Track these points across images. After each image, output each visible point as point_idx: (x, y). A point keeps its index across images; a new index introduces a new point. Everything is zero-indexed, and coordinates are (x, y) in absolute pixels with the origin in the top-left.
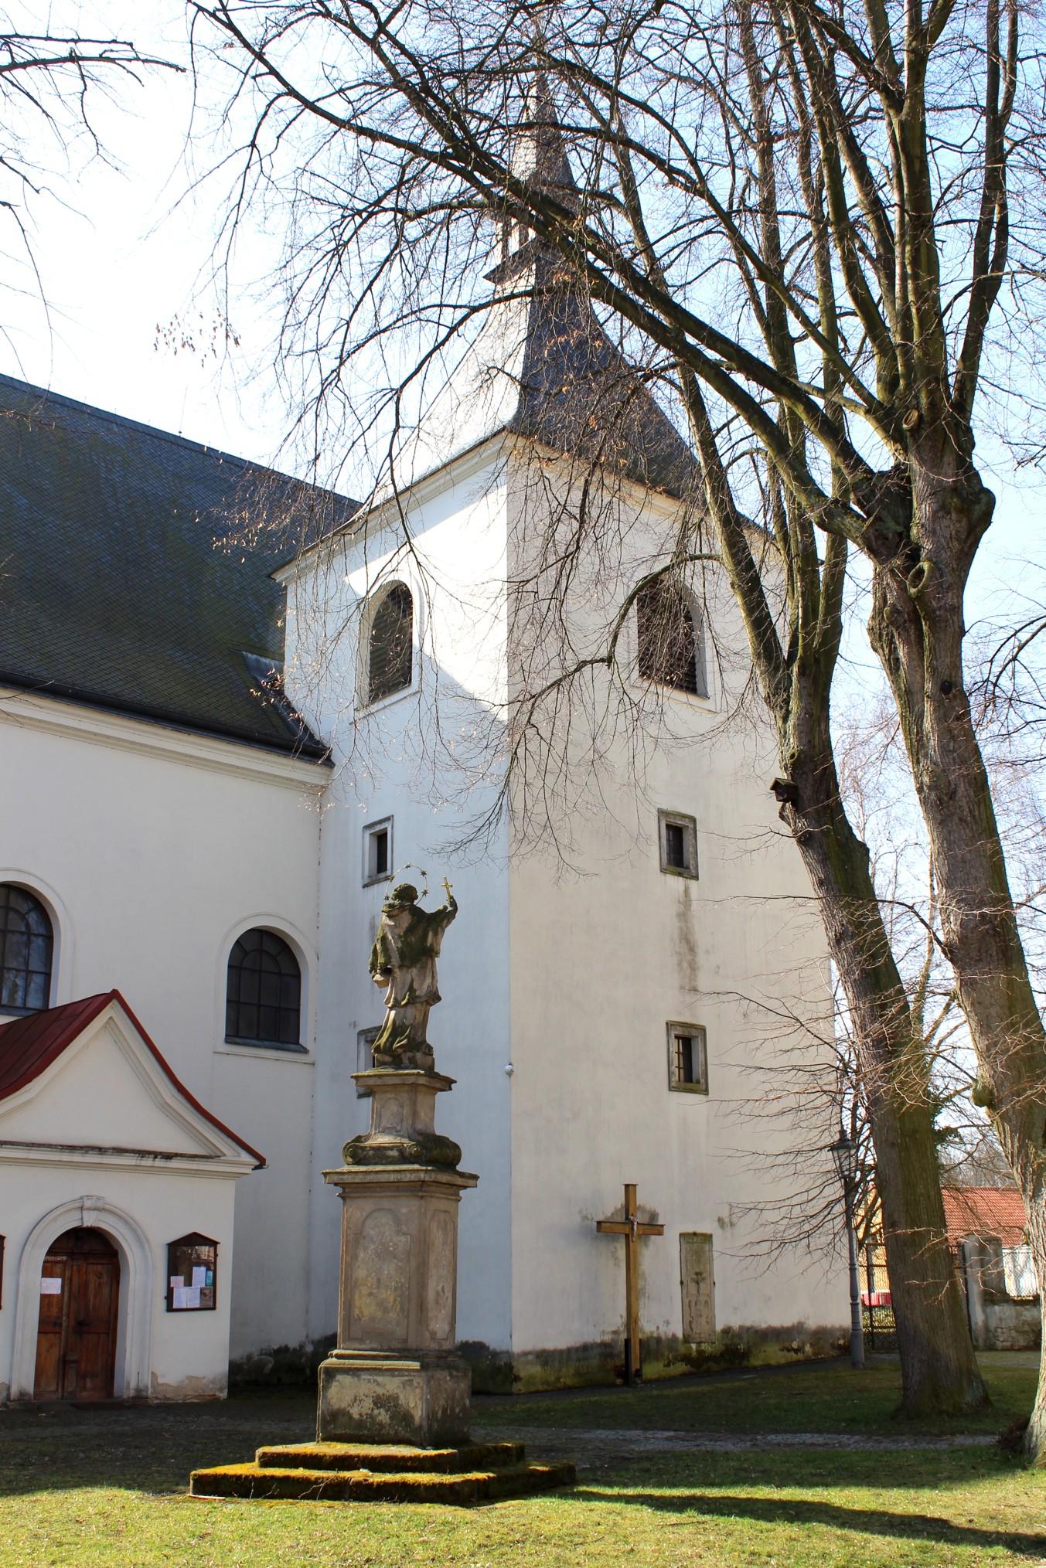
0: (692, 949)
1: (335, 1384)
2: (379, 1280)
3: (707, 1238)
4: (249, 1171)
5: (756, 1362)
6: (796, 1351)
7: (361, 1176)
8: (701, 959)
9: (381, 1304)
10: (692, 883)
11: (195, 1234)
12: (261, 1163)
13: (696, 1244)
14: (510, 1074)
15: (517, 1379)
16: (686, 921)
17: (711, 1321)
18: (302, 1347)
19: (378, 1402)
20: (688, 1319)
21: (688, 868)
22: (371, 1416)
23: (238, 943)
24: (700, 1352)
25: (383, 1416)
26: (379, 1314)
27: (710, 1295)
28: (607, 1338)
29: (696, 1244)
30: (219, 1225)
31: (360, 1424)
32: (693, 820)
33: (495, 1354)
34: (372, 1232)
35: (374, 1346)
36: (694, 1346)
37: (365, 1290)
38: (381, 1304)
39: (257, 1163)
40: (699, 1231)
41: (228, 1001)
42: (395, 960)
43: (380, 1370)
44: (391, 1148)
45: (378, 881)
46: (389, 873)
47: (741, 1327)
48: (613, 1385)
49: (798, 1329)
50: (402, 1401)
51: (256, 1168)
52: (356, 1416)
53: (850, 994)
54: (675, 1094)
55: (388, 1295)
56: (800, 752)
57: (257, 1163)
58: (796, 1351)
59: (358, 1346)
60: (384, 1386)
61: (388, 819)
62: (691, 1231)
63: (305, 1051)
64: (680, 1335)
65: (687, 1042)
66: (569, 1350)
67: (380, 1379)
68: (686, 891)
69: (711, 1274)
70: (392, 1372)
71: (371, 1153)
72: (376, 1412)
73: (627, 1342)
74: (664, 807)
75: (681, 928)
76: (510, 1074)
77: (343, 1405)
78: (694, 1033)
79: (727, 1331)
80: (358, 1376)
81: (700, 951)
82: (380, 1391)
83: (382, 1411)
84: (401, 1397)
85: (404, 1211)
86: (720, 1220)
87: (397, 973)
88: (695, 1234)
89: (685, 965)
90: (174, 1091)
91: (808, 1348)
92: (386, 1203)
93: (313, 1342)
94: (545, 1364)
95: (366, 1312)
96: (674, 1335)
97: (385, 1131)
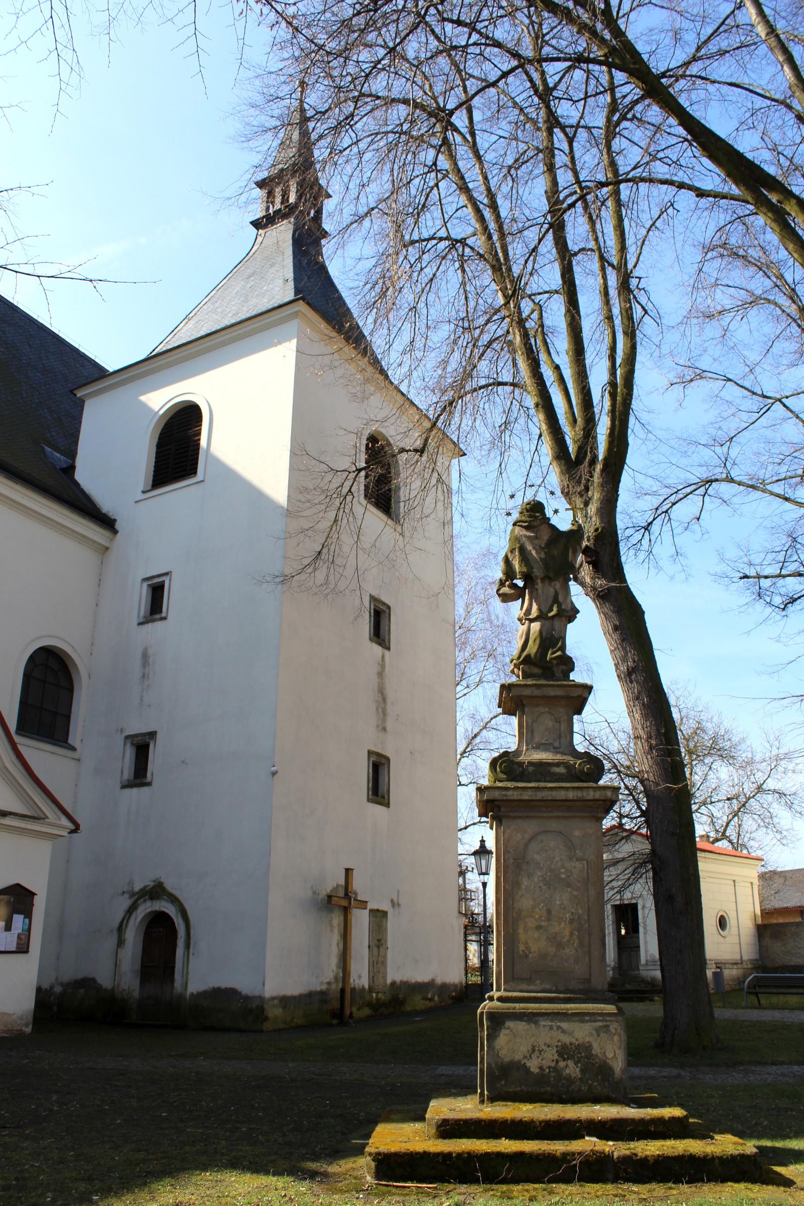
0: (384, 700)
1: (504, 1032)
2: (549, 911)
3: (384, 914)
4: (65, 834)
5: (408, 1008)
6: (430, 1000)
7: (530, 793)
8: (389, 708)
9: (554, 939)
10: (386, 652)
11: (18, 885)
12: (76, 829)
13: (379, 916)
14: (274, 774)
15: (266, 1019)
16: (382, 679)
17: (385, 978)
18: (52, 987)
19: (565, 1052)
20: (372, 974)
21: (384, 641)
22: (555, 1069)
23: (32, 658)
24: (378, 999)
25: (572, 1069)
26: (552, 950)
27: (385, 957)
28: (324, 987)
29: (379, 916)
30: (37, 882)
31: (541, 1078)
32: (389, 608)
33: (247, 998)
34: (537, 857)
35: (548, 987)
36: (374, 995)
37: (531, 923)
38: (554, 939)
39: (73, 827)
40: (381, 908)
41: (21, 702)
42: (538, 572)
43: (565, 1014)
44: (558, 765)
45: (154, 621)
46: (164, 615)
47: (401, 982)
48: (331, 1025)
49: (430, 985)
50: (596, 1049)
51: (72, 832)
52: (534, 1069)
53: (637, 716)
54: (371, 804)
55: (564, 930)
56: (603, 528)
57: (73, 827)
58: (430, 1000)
59: (525, 987)
60: (571, 1034)
61: (167, 574)
62: (376, 908)
63: (73, 749)
64: (367, 987)
65: (378, 766)
66: (300, 996)
67: (565, 1025)
68: (383, 657)
69: (386, 941)
70: (580, 1017)
71: (531, 769)
72: (562, 1064)
73: (343, 991)
74: (373, 594)
75: (379, 683)
76: (274, 774)
77: (518, 1057)
78: (383, 761)
79: (393, 984)
80: (536, 1023)
81: (389, 701)
82: (566, 1039)
83: (571, 1063)
84: (595, 1045)
85: (577, 833)
86: (392, 901)
87: (539, 585)
88: (378, 910)
89: (380, 710)
90: (14, 757)
91: (436, 998)
92: (554, 825)
93: (62, 984)
94: (284, 1007)
95: (534, 948)
96: (363, 987)
97: (538, 747)
